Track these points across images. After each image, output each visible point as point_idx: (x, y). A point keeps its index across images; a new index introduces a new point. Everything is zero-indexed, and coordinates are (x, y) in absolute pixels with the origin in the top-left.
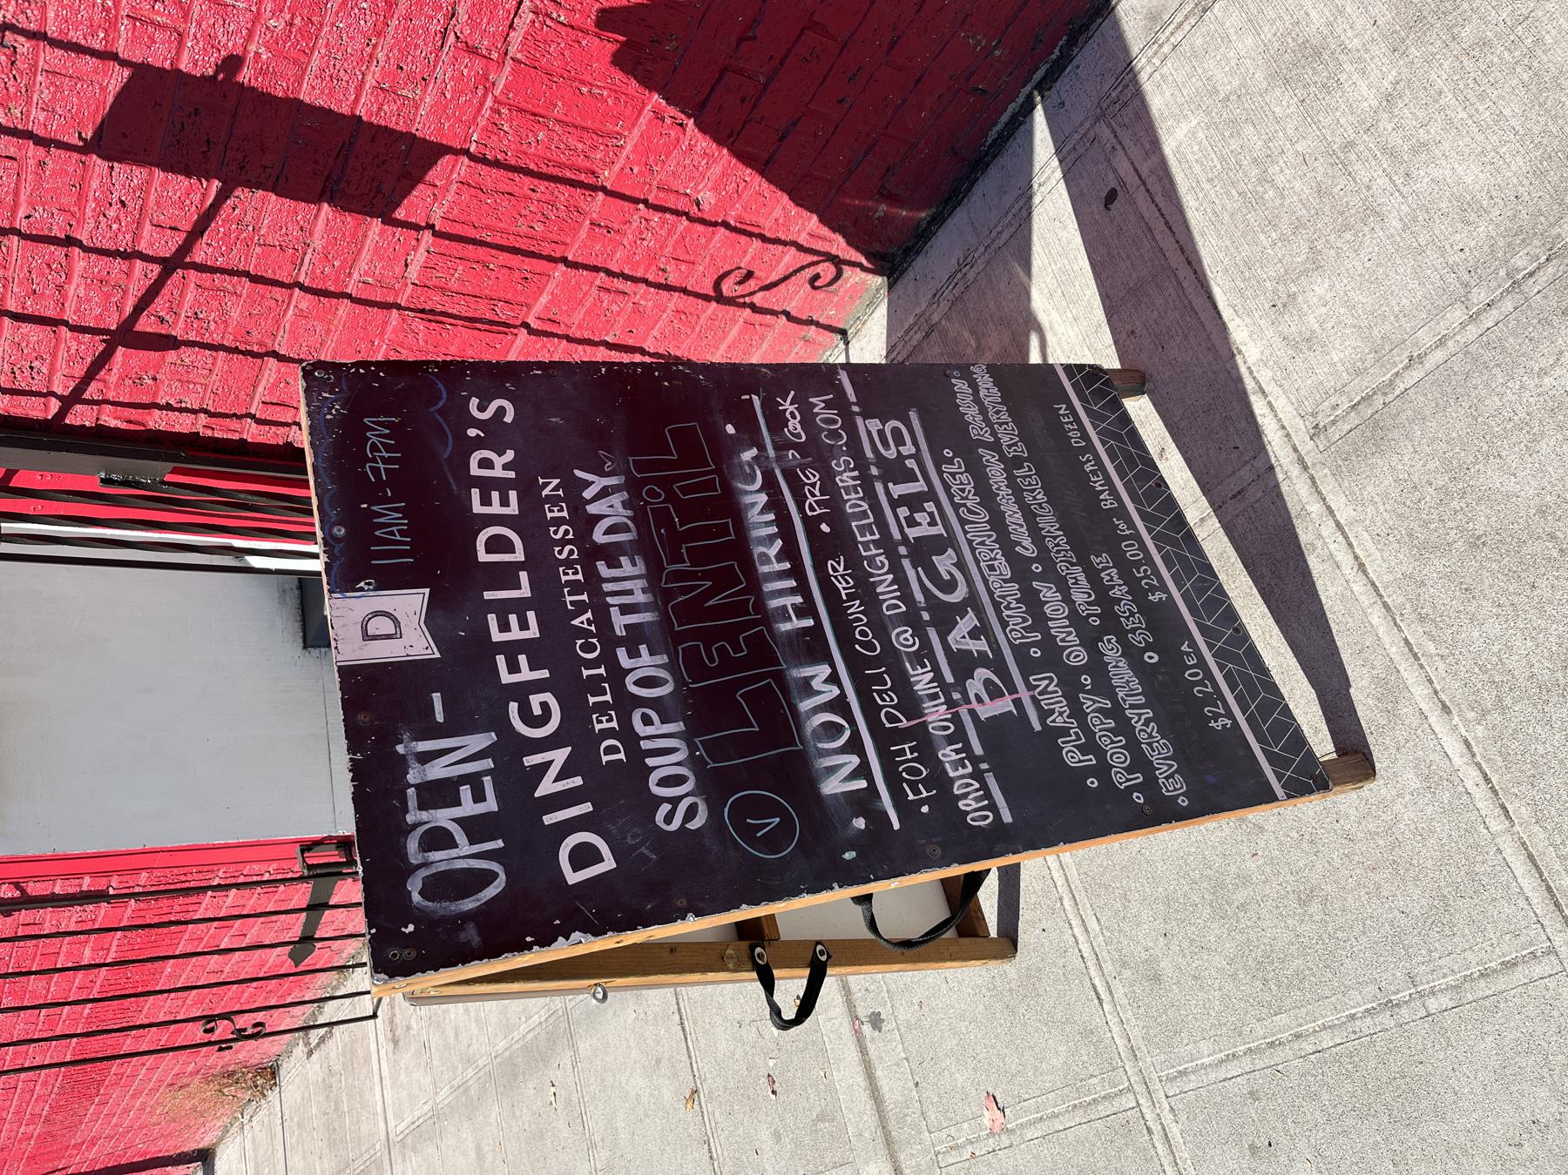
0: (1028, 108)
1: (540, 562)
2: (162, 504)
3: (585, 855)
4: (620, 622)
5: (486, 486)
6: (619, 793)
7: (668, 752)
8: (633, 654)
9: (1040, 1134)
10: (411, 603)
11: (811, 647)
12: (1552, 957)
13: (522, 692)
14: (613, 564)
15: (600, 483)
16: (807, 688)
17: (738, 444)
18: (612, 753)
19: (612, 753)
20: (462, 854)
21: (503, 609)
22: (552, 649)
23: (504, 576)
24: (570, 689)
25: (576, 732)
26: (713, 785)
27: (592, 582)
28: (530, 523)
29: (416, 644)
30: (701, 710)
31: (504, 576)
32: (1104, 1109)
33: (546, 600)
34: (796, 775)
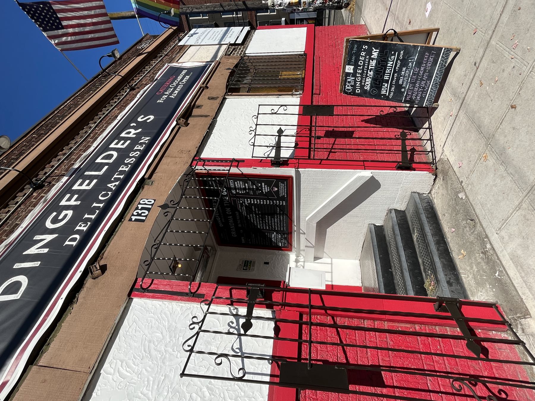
1: (364, 65)
3: (358, 91)
4: (370, 68)
5: (362, 56)
6: (362, 87)
7: (369, 81)
8: (370, 71)
9: (362, 158)
10: (352, 67)
11: (387, 81)
12: (399, 158)
13: (358, 77)
14: (372, 61)
15: (375, 50)
16: (384, 85)
17: (392, 55)
18: (363, 84)
19: (363, 84)
20: (350, 88)
21: (359, 69)
22: (362, 74)
23: (360, 66)
24: (362, 78)
25: (361, 81)
26: (371, 87)
27: (369, 62)
29: (352, 71)
30: (374, 79)
31: (360, 66)
32: (467, 19)
33: (363, 69)
34: (380, 88)
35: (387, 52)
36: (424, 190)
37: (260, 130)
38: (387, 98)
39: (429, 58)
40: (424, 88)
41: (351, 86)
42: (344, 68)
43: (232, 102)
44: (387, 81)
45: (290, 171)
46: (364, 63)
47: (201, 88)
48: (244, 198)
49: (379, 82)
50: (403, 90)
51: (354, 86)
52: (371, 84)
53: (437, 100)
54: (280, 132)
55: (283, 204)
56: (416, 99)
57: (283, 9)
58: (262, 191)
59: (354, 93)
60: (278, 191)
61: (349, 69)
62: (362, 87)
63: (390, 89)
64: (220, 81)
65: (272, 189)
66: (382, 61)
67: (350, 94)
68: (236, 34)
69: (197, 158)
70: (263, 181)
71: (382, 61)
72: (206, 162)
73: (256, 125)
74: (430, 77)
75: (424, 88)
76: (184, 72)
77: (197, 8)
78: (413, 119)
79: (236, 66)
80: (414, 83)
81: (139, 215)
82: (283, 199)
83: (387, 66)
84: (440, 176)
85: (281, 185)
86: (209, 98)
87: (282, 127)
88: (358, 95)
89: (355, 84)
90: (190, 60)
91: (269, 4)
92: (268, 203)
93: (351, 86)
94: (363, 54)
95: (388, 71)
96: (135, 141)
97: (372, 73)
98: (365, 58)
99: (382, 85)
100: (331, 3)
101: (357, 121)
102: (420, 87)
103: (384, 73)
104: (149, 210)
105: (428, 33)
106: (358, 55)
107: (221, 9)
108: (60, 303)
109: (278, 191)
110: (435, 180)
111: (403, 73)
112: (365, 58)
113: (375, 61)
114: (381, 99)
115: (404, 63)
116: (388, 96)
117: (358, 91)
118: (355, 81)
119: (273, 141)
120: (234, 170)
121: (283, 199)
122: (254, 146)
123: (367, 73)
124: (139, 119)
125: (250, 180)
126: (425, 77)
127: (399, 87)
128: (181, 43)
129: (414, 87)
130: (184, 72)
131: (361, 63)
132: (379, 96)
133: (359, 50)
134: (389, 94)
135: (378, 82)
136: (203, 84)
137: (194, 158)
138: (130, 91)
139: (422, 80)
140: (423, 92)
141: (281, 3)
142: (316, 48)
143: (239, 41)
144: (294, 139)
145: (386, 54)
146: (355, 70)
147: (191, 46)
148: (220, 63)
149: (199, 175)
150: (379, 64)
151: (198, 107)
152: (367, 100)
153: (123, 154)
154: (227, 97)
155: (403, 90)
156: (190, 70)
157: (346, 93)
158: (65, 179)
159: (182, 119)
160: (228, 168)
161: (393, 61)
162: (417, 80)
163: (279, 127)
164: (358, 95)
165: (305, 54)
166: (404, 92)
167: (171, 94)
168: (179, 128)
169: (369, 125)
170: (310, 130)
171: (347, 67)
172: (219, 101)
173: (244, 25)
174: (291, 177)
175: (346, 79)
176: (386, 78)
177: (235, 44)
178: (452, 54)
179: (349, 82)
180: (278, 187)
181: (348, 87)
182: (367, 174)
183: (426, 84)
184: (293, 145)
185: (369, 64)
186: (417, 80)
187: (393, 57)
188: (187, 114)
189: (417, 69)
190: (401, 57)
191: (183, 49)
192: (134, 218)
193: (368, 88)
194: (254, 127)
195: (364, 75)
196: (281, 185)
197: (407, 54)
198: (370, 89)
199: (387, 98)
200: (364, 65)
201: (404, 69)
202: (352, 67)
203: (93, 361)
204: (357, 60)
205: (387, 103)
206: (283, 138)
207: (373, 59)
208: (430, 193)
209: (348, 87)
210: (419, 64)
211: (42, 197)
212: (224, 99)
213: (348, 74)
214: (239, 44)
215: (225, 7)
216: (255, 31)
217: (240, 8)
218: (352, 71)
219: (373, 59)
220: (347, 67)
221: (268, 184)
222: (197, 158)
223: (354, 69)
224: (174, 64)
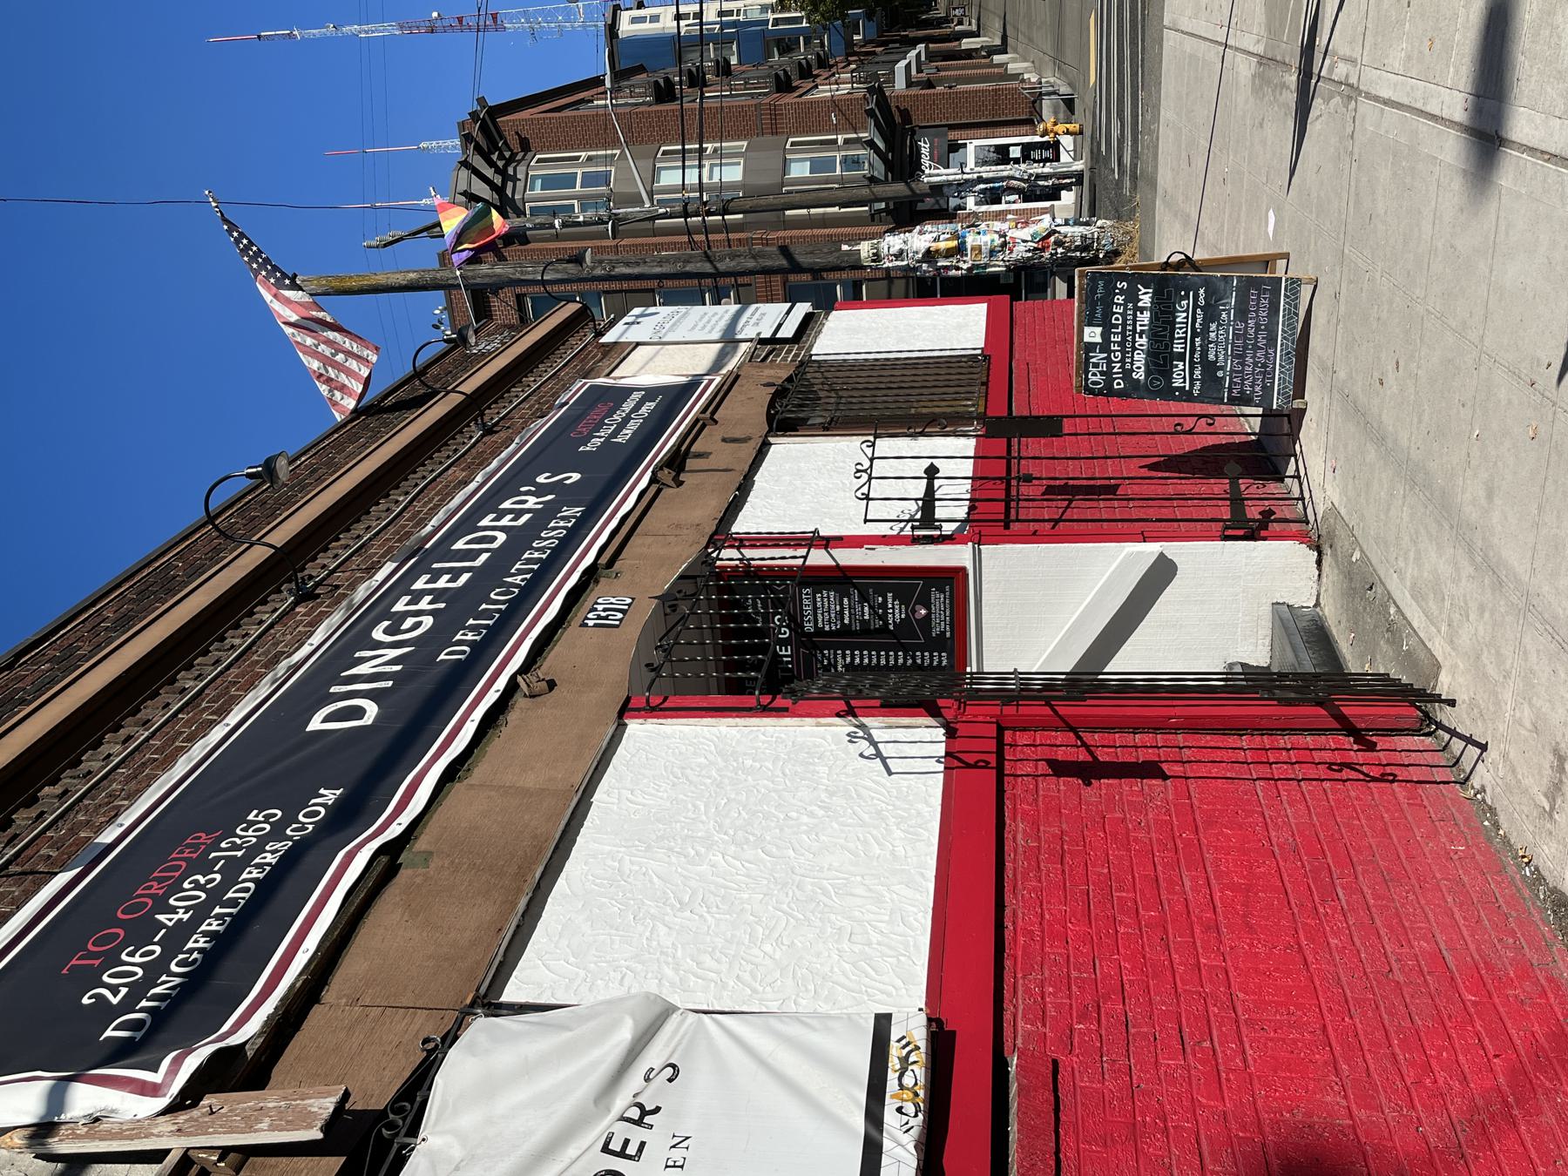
0: (913, 43)
1: (1124, 325)
2: (649, 1027)
4: (1139, 329)
6: (1126, 374)
7: (1140, 359)
10: (1099, 330)
11: (1181, 357)
17: (1183, 298)
18: (1128, 366)
19: (1128, 366)
20: (1098, 378)
22: (1122, 344)
23: (1116, 326)
24: (1124, 352)
25: (1123, 361)
26: (1148, 372)
27: (1135, 316)
28: (1124, 315)
29: (1098, 339)
30: (1152, 355)
31: (1116, 326)
33: (1123, 333)
34: (1168, 375)
35: (1169, 293)
36: (1303, 598)
37: (877, 489)
38: (1187, 396)
39: (1259, 299)
40: (1264, 366)
41: (1102, 373)
42: (1081, 333)
43: (784, 450)
44: (1181, 357)
45: (958, 556)
46: (1125, 320)
47: (697, 421)
48: (835, 647)
49: (1165, 359)
50: (1220, 374)
51: (1108, 374)
52: (1147, 365)
53: (1300, 391)
54: (932, 472)
55: (940, 662)
56: (1253, 392)
57: (907, 268)
58: (886, 624)
59: (1108, 391)
60: (928, 615)
61: (1093, 334)
62: (1126, 374)
63: (1191, 374)
64: (748, 408)
65: (913, 611)
66: (1163, 312)
67: (1100, 393)
68: (769, 318)
69: (721, 534)
70: (891, 588)
71: (1163, 312)
72: (742, 542)
73: (872, 460)
74: (1272, 341)
75: (1264, 366)
76: (636, 396)
77: (627, 264)
78: (1269, 455)
79: (790, 379)
80: (1242, 357)
81: (599, 618)
82: (939, 643)
83: (1175, 323)
84: (1327, 550)
85: (939, 599)
86: (724, 440)
87: (935, 462)
88: (1120, 394)
89: (1110, 368)
90: (646, 370)
91: (864, 254)
92: (901, 661)
93: (1102, 373)
94: (1119, 299)
95: (1179, 334)
96: (542, 518)
97: (1144, 340)
98: (1126, 309)
99: (1172, 366)
100: (1060, 250)
101: (1131, 468)
102: (1256, 364)
103: (1172, 338)
104: (624, 612)
105: (1267, 262)
106: (1108, 304)
107: (708, 268)
108: (470, 729)
109: (928, 615)
110: (1319, 562)
111: (1212, 335)
112: (1126, 309)
113: (1147, 314)
114: (1175, 399)
115: (1211, 314)
116: (1191, 391)
117: (1118, 385)
118: (1109, 362)
119: (919, 489)
120: (818, 558)
121: (939, 643)
122: (867, 498)
123: (1134, 341)
124: (541, 479)
125: (855, 586)
126: (1262, 343)
127: (1210, 368)
128: (608, 338)
129: (1243, 364)
130: (636, 396)
131: (1116, 319)
132: (1168, 393)
133: (1110, 292)
134: (1192, 385)
135: (1161, 360)
136: (704, 411)
137: (711, 537)
138: (482, 436)
139: (1256, 348)
140: (1264, 373)
141: (901, 252)
142: (1016, 346)
143: (788, 331)
144: (967, 485)
145: (1169, 297)
146: (1106, 335)
147: (638, 344)
148: (738, 377)
149: (723, 573)
150: (1157, 319)
151: (699, 456)
152: (1147, 405)
153: (520, 539)
154: (771, 440)
155: (1220, 374)
156: (651, 393)
157: (1091, 392)
158: (389, 567)
159: (666, 471)
160: (802, 552)
161: (1187, 311)
162: (1245, 348)
163: (927, 463)
164: (1120, 394)
165: (986, 356)
166: (1223, 378)
167: (615, 434)
168: (659, 491)
169: (1154, 474)
170: (1008, 509)
171: (1087, 330)
172: (749, 451)
173: (792, 298)
174: (962, 571)
175: (1088, 358)
176: (1178, 348)
177: (773, 340)
178: (1306, 292)
179: (1096, 365)
180: (928, 607)
181: (1095, 378)
182: (1152, 549)
183: (1266, 356)
184: (941, 750)
185: (1135, 321)
186: (1245, 348)
187: (1184, 303)
188: (677, 461)
189: (1241, 326)
190: (1202, 302)
191: (621, 351)
192: (591, 623)
193: (1140, 375)
194: (866, 464)
195: (1127, 348)
196: (939, 599)
197: (1214, 293)
198: (1147, 377)
199: (1187, 396)
200: (1124, 325)
201: (1213, 326)
202: (1099, 330)
203: (579, 778)
204: (1108, 314)
205: (1186, 407)
206: (937, 483)
207: (1142, 310)
208: (1317, 604)
209: (1095, 378)
210: (1242, 313)
211: (345, 596)
212: (764, 447)
213: (1090, 347)
214: (785, 341)
215: (722, 259)
216: (827, 314)
217: (769, 263)
218: (1098, 339)
219: (1142, 310)
220: (1087, 330)
221: (903, 596)
222: (721, 534)
223: (1102, 335)
224: (601, 381)
